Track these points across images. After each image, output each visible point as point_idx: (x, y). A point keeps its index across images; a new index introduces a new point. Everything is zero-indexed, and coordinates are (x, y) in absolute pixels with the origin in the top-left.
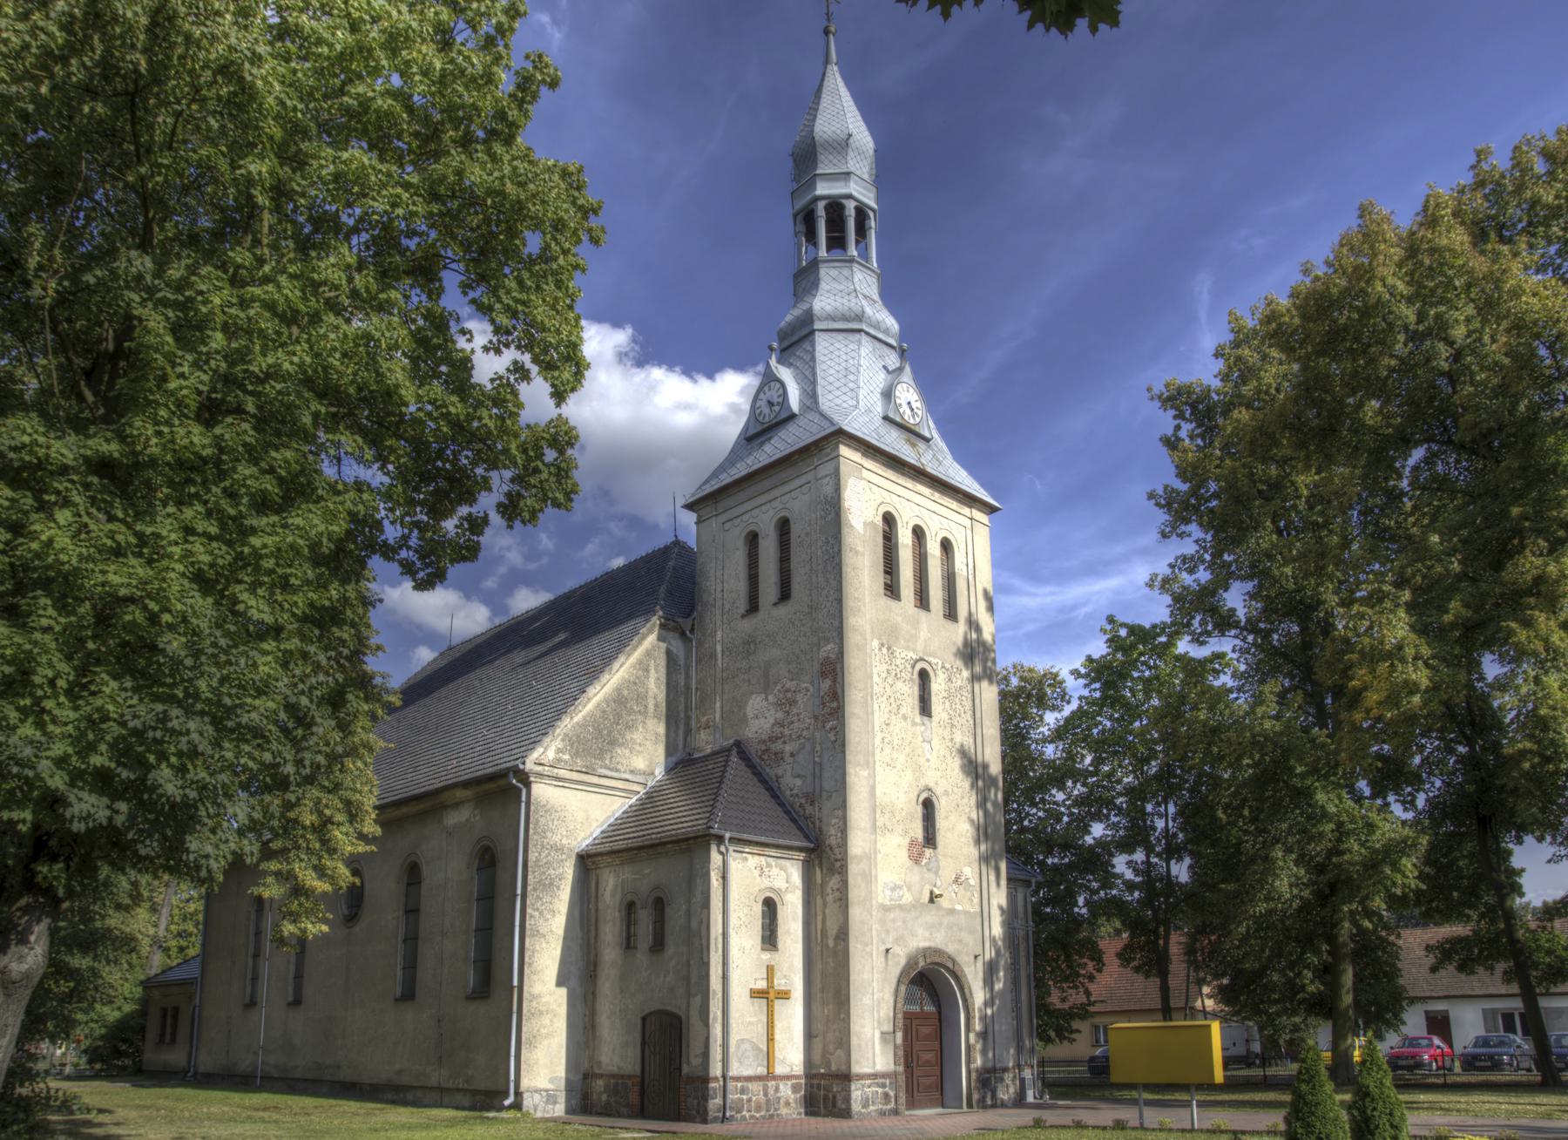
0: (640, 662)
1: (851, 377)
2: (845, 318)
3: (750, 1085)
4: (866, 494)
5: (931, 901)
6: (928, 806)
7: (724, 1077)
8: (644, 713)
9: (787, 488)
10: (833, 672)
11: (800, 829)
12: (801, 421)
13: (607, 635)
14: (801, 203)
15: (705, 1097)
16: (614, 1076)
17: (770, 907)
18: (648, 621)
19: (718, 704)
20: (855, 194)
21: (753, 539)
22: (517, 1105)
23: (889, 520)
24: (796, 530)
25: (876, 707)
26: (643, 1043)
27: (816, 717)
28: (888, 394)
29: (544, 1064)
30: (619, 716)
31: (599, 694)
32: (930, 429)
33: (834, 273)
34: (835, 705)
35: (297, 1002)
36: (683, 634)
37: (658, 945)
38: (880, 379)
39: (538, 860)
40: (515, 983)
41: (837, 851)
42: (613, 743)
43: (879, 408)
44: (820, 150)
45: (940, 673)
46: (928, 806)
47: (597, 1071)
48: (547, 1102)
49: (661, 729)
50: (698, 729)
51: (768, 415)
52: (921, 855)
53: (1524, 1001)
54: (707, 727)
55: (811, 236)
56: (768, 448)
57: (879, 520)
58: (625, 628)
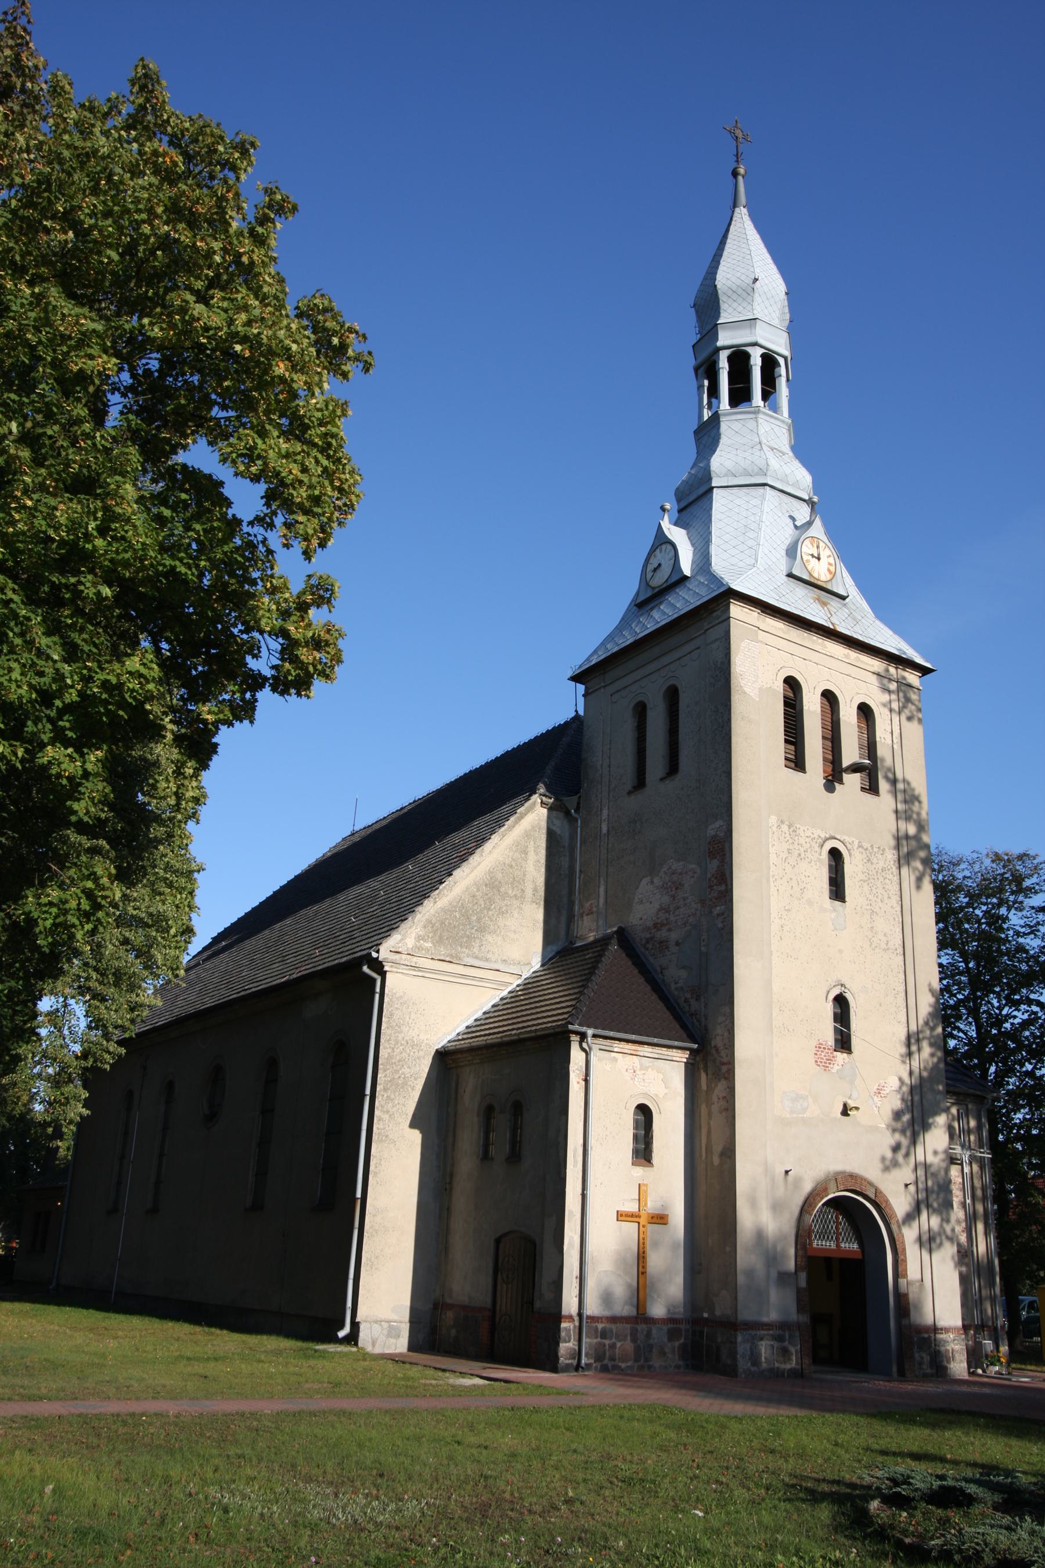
0: (517, 844)
1: (751, 534)
4: (759, 660)
5: (845, 1112)
6: (841, 1002)
8: (521, 897)
9: (676, 655)
10: (719, 851)
11: (684, 1026)
12: (690, 585)
13: (488, 817)
14: (704, 355)
15: (555, 1339)
16: (464, 1307)
18: (527, 799)
19: (602, 889)
20: (761, 341)
21: (641, 710)
22: (353, 1338)
23: (792, 684)
24: (685, 700)
25: (773, 890)
26: (496, 1270)
27: (703, 902)
28: (792, 552)
29: (384, 1291)
30: (491, 901)
31: (465, 880)
32: (845, 584)
33: (736, 426)
34: (723, 888)
35: (154, 1210)
36: (567, 813)
37: (514, 1156)
38: (788, 533)
39: (390, 1057)
40: (359, 1195)
41: (723, 1053)
42: (482, 930)
43: (783, 567)
44: (722, 298)
45: (856, 853)
46: (841, 1002)
47: (449, 1301)
48: (389, 1335)
49: (539, 914)
50: (582, 916)
51: (659, 580)
52: (830, 1060)
54: (590, 913)
55: (714, 392)
56: (656, 614)
57: (779, 687)
58: (505, 808)
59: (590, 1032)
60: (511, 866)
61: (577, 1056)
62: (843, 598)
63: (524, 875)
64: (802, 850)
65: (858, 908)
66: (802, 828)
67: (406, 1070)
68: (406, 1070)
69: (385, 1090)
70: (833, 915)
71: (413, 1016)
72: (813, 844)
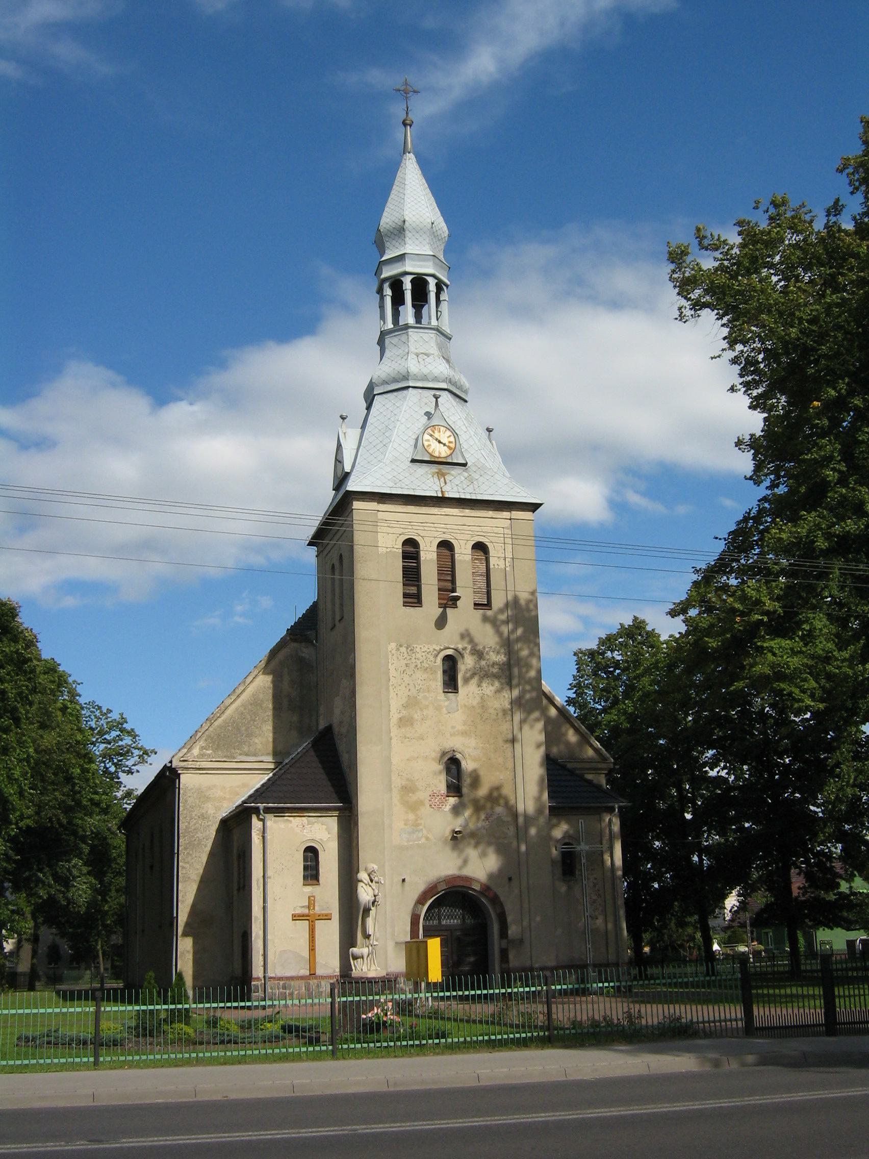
2: (395, 380)
3: (292, 983)
7: (264, 977)
17: (311, 854)
33: (395, 340)
53: (708, 925)
61: (256, 824)
62: (465, 465)
64: (418, 662)
65: (471, 694)
66: (419, 647)
67: (199, 835)
68: (199, 835)
69: (186, 849)
72: (429, 656)
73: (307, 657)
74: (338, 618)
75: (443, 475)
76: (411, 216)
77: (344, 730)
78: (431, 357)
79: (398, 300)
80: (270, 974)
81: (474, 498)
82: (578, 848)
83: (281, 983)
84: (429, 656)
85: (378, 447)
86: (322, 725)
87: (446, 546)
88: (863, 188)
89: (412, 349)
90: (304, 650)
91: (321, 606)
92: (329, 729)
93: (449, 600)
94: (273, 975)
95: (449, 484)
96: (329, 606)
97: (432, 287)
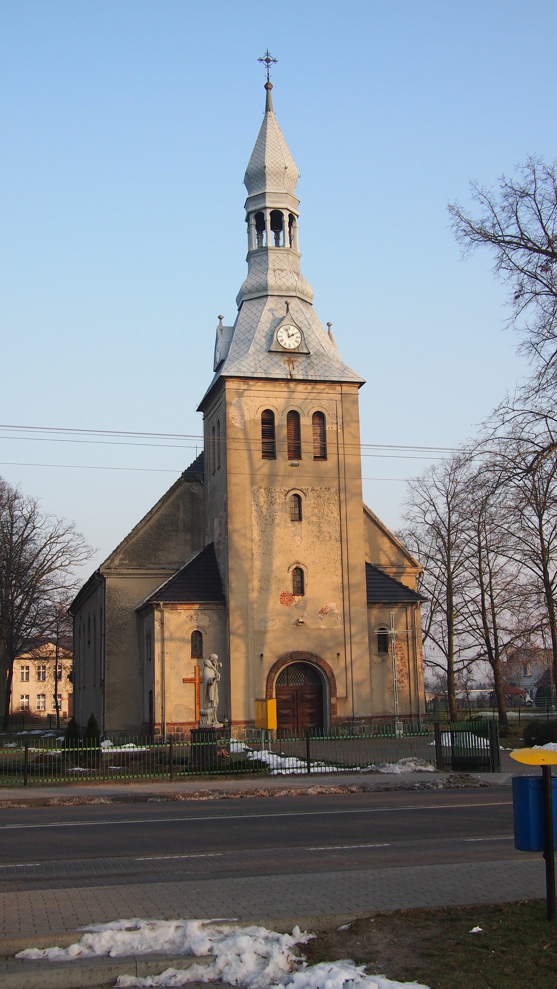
2: (258, 290)
3: (183, 727)
45: (310, 494)
59: (162, 603)
60: (170, 516)
61: (157, 614)
63: (178, 519)
66: (273, 489)
70: (293, 529)
71: (121, 596)
73: (197, 493)
74: (217, 467)
75: (292, 362)
76: (270, 163)
77: (221, 548)
78: (285, 272)
79: (260, 227)
80: (167, 720)
81: (314, 379)
82: (390, 632)
83: (176, 727)
84: (281, 495)
85: (245, 342)
86: (208, 542)
87: (294, 417)
88: (41, 579)
89: (271, 266)
90: (194, 487)
91: (206, 455)
92: (212, 545)
93: (296, 453)
94: (170, 722)
95: (296, 369)
96: (211, 457)
97: (286, 219)
